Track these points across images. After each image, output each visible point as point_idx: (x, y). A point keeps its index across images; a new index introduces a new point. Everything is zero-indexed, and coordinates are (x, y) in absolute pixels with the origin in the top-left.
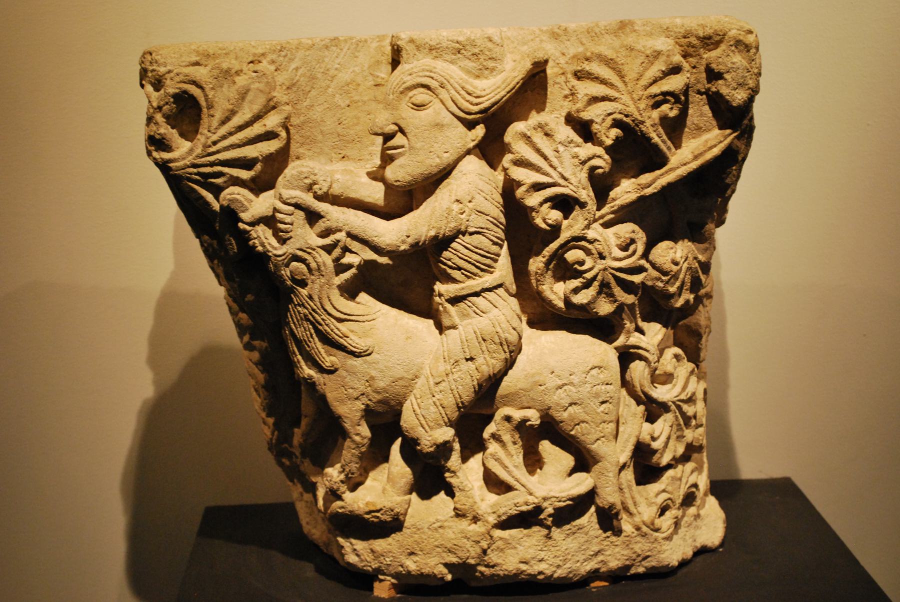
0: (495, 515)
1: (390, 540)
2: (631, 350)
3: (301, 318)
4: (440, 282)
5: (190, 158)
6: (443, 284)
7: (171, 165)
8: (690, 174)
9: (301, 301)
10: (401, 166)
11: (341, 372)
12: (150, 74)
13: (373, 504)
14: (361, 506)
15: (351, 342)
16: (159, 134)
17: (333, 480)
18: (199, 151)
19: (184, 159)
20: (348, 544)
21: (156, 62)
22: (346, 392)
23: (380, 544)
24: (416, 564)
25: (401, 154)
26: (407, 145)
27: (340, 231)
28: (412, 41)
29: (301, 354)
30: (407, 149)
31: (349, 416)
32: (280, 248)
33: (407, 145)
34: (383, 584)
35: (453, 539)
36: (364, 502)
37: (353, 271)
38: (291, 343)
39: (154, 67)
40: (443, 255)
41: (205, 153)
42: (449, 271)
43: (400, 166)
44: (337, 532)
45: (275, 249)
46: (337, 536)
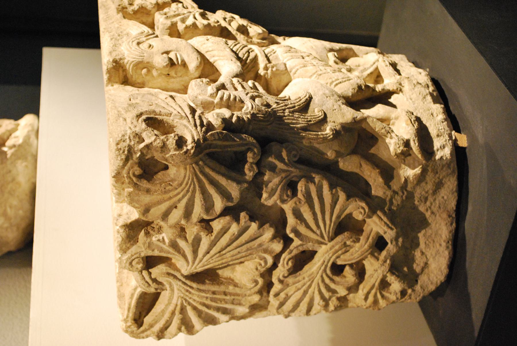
0: (396, 75)
1: (428, 125)
2: (291, 125)
3: (292, 116)
4: (258, 70)
5: (190, 127)
6: (259, 69)
7: (196, 140)
8: (194, 282)
9: (281, 110)
10: (188, 56)
11: (324, 108)
12: (132, 143)
13: (406, 121)
14: (410, 128)
15: (303, 97)
16: (175, 137)
17: (397, 141)
18: (185, 122)
19: (191, 131)
20: (439, 153)
21: (123, 136)
22: (337, 110)
23: (433, 131)
24: (439, 115)
25: (181, 56)
26: (175, 52)
27: (232, 81)
28: (110, 53)
29: (318, 132)
30: (177, 52)
31: (352, 113)
32: (247, 105)
33: (175, 52)
34: (458, 138)
35: (417, 95)
36: (407, 127)
37: (257, 84)
38: (311, 135)
39: (127, 138)
40: (242, 57)
41: (186, 118)
42: (250, 58)
43: (188, 57)
44: (433, 159)
45: (248, 108)
46: (435, 159)
